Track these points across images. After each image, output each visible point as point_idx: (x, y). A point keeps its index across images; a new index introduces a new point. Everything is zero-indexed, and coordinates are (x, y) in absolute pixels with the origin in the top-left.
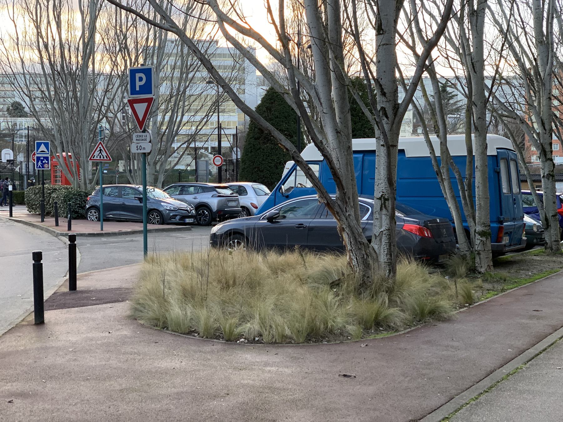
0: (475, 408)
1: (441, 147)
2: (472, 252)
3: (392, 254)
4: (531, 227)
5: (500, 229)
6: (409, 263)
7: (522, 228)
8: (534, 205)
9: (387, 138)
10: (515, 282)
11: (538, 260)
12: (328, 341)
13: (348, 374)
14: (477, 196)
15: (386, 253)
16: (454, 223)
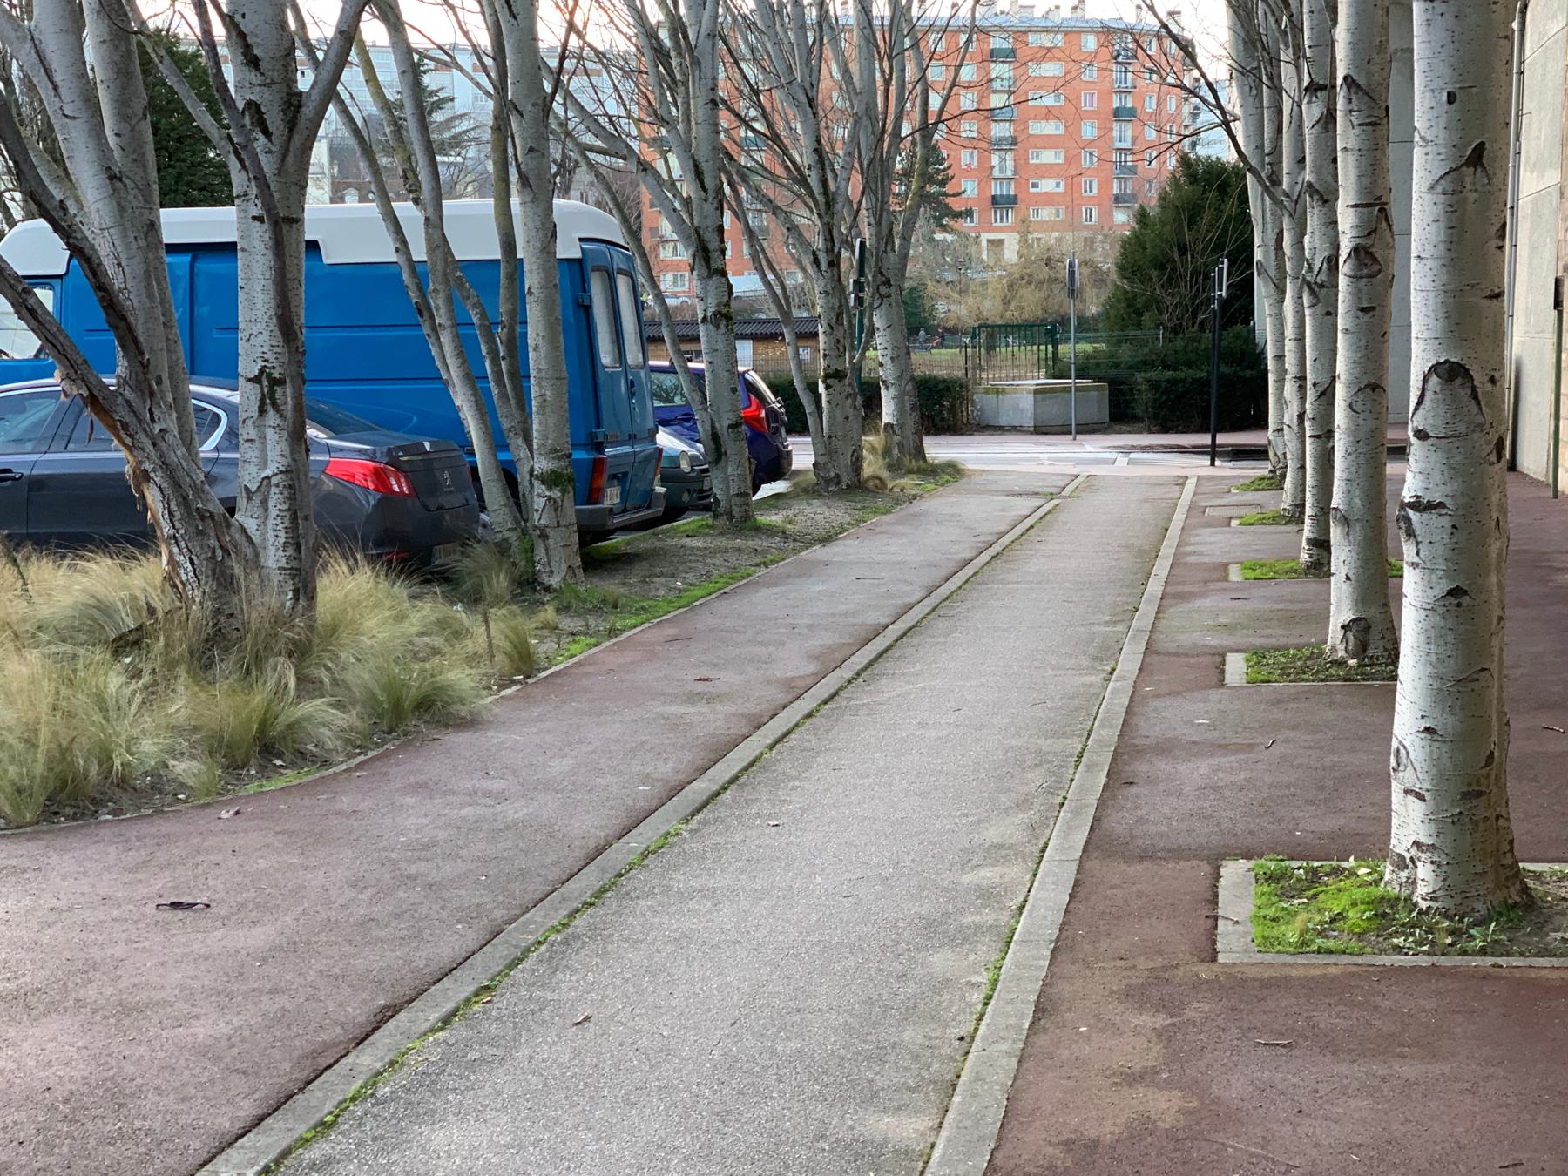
0: (563, 952)
1: (427, 233)
2: (524, 532)
3: (302, 542)
4: (675, 459)
5: (598, 465)
6: (352, 571)
7: (654, 461)
8: (678, 401)
9: (272, 195)
10: (643, 608)
11: (699, 549)
12: (115, 813)
13: (185, 899)
14: (533, 373)
15: (282, 540)
16: (472, 453)
